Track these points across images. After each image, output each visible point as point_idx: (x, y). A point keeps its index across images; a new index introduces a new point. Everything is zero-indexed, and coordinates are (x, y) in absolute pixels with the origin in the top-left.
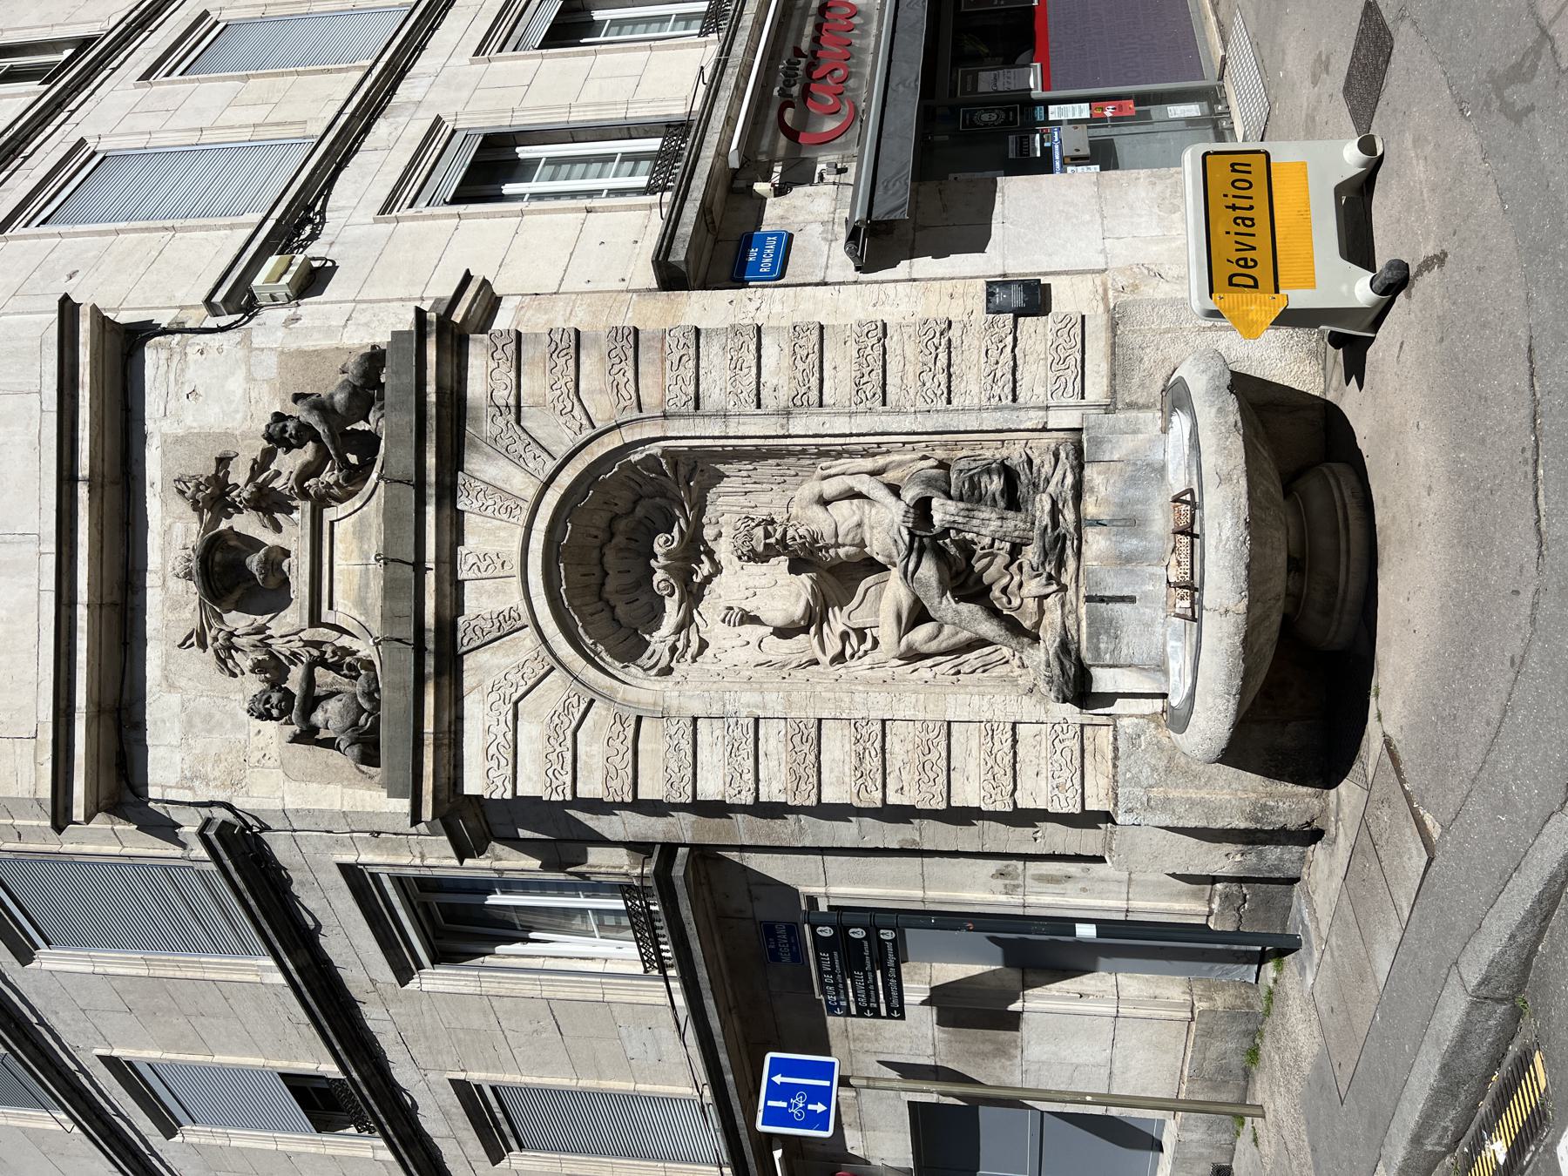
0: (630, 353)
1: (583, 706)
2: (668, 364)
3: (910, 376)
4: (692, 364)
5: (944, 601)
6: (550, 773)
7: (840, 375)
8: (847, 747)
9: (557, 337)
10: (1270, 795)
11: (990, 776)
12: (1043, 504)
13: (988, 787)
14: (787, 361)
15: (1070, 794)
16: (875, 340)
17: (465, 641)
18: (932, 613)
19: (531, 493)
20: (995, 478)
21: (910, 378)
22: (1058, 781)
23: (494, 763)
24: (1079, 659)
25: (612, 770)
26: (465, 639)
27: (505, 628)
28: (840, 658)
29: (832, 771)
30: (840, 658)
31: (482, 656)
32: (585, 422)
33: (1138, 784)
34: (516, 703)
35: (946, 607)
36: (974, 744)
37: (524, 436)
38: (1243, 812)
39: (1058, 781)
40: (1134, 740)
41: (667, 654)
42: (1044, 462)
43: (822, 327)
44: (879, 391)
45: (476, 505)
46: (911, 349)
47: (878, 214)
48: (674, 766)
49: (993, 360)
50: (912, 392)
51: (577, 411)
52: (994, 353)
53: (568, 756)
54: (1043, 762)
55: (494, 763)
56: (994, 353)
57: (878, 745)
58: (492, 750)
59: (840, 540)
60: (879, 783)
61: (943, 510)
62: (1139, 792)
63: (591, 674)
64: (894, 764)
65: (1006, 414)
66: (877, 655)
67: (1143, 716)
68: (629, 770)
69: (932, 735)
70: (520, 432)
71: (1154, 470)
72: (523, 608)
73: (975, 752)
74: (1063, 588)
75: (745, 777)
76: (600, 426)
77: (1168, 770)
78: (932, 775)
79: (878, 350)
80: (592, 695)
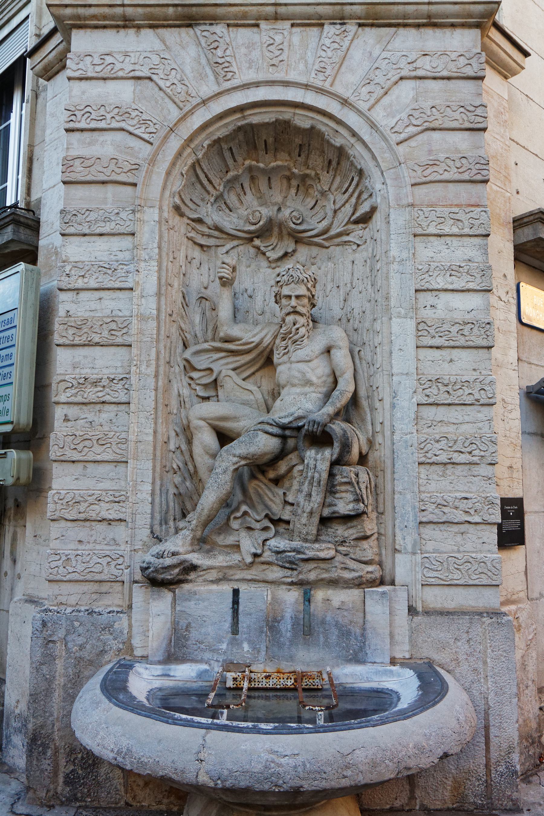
0: (466, 176)
1: (146, 136)
2: (456, 210)
3: (445, 429)
5: (235, 459)
6: (88, 109)
7: (446, 365)
8: (106, 371)
9: (479, 111)
10: (56, 751)
12: (325, 550)
13: (69, 498)
14: (458, 316)
16: (477, 396)
17: (205, 34)
18: (225, 448)
19: (339, 89)
23: (97, 61)
24: (180, 582)
25: (88, 163)
27: (220, 68)
28: (189, 367)
29: (85, 357)
30: (189, 367)
32: (403, 136)
33: (68, 633)
34: (150, 79)
35: (230, 458)
38: (42, 727)
41: (195, 216)
44: (431, 400)
45: (327, 42)
46: (466, 428)
48: (93, 216)
50: (430, 430)
51: (412, 130)
53: (102, 125)
54: (90, 546)
55: (97, 61)
56: (463, 505)
57: (107, 398)
58: (109, 59)
59: (294, 365)
60: (73, 399)
61: (318, 460)
63: (175, 144)
67: (130, 638)
68: (89, 178)
70: (394, 79)
71: (356, 654)
72: (236, 82)
73: (101, 486)
75: (80, 281)
77: (79, 659)
78: (80, 447)
79: (469, 400)
80: (156, 144)
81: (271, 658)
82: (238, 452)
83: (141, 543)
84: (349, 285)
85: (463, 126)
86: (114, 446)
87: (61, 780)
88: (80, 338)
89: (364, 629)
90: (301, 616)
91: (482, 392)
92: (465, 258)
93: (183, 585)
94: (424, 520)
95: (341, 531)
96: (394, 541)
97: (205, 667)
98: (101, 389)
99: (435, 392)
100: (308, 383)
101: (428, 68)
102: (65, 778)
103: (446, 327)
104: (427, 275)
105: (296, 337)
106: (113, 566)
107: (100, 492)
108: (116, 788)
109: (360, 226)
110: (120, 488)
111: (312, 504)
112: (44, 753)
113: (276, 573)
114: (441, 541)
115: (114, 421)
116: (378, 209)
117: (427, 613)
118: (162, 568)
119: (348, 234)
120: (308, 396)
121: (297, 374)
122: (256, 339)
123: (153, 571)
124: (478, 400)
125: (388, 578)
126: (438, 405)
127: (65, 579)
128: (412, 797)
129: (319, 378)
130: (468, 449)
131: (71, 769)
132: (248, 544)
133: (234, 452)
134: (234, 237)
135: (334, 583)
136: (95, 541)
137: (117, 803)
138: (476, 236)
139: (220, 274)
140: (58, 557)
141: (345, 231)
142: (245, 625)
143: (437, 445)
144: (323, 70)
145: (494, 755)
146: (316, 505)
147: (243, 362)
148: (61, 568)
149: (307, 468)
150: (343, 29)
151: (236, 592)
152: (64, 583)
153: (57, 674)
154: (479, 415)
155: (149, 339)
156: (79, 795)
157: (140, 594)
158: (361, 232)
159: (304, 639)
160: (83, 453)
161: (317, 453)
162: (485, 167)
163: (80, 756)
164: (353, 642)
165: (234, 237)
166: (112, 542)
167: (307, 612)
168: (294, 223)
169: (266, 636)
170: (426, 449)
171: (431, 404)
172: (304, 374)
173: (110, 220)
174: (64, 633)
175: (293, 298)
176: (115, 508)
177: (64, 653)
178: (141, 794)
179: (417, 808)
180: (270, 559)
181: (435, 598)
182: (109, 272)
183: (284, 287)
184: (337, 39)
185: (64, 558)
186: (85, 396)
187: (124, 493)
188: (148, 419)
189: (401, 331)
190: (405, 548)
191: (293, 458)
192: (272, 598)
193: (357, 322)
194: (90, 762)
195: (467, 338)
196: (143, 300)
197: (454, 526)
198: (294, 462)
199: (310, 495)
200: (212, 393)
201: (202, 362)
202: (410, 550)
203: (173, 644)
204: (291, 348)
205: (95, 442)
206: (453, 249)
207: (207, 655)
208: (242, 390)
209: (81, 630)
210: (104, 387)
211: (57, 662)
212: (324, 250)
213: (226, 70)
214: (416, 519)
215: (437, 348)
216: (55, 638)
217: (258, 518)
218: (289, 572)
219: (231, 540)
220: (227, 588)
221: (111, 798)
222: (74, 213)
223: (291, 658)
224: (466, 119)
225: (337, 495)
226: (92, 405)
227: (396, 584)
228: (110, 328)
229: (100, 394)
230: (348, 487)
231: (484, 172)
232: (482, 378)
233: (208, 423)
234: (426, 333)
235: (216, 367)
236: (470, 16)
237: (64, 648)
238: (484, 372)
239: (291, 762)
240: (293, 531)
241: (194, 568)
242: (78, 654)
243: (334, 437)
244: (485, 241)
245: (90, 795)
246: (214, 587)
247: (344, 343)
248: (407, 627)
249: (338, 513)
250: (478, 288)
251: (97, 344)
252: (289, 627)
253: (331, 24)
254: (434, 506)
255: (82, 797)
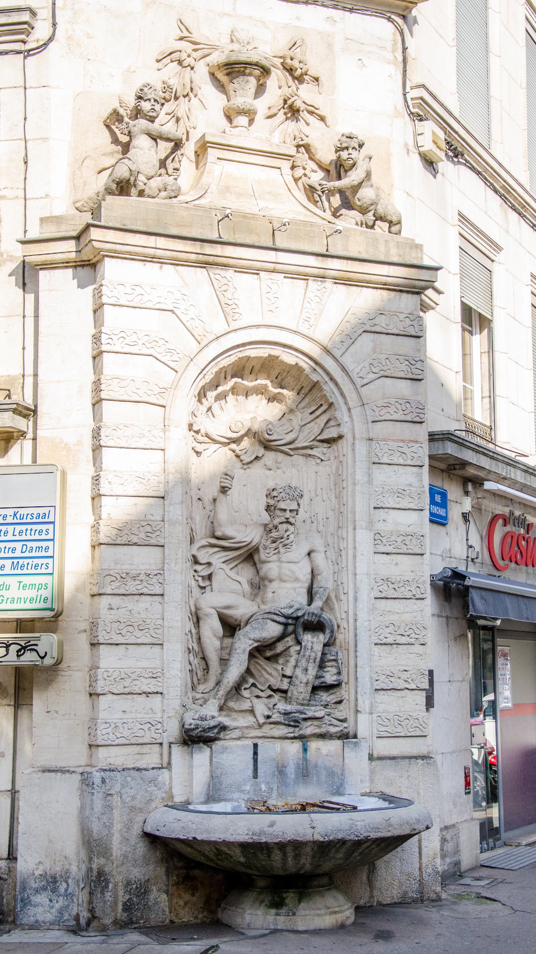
0: (409, 418)
1: (172, 364)
4: (401, 461)
8: (142, 567)
9: (419, 365)
10: (116, 885)
11: (123, 676)
13: (116, 675)
15: (111, 736)
16: (414, 593)
17: (217, 277)
20: (335, 678)
21: (394, 618)
22: (121, 726)
26: (217, 273)
27: (227, 309)
30: (196, 561)
31: (207, 289)
32: (366, 381)
33: (123, 786)
36: (145, 664)
37: (356, 335)
39: (121, 726)
40: (153, 781)
42: (340, 712)
43: (422, 555)
44: (383, 595)
46: (407, 617)
47: (474, 595)
49: (400, 675)
50: (381, 618)
51: (372, 376)
52: (405, 676)
54: (133, 715)
56: (405, 676)
57: (145, 591)
58: (139, 290)
59: (284, 565)
62: (117, 787)
64: (128, 603)
65: (368, 685)
66: (196, 591)
67: (171, 788)
69: (152, 632)
70: (359, 332)
71: (338, 788)
74: (260, 726)
76: (363, 391)
77: (132, 809)
78: (124, 632)
81: (280, 795)
82: (252, 636)
83: (174, 711)
84: (313, 493)
85: (407, 377)
86: (152, 632)
87: (120, 907)
88: (121, 539)
89: (343, 770)
90: (301, 762)
91: (418, 589)
92: (407, 483)
93: (217, 742)
94: (378, 687)
95: (324, 696)
96: (356, 705)
97: (236, 804)
98: (140, 583)
99: (386, 588)
100: (297, 580)
101: (384, 325)
102: (123, 906)
103: (394, 538)
104: (381, 496)
105: (287, 542)
106: (153, 731)
107: (140, 670)
108: (163, 909)
109: (325, 445)
110: (155, 666)
111: (308, 677)
112: (107, 887)
113: (282, 731)
114: (388, 703)
115: (149, 609)
116: (345, 438)
117: (380, 758)
118: (209, 728)
119: (312, 449)
120: (297, 591)
121: (288, 573)
122: (248, 539)
123: (201, 731)
124: (414, 596)
125: (351, 733)
126: (387, 598)
127: (114, 744)
128: (372, 897)
129: (305, 576)
130: (408, 633)
131: (128, 898)
132: (261, 708)
133: (250, 636)
134: (215, 441)
135: (322, 736)
136: (136, 712)
137: (163, 922)
138: (415, 466)
139: (223, 484)
140: (108, 725)
141: (311, 446)
142: (262, 771)
143: (387, 630)
144: (308, 319)
145: (424, 861)
146: (311, 677)
147: (231, 556)
148: (111, 734)
149: (305, 649)
150: (323, 286)
151: (256, 746)
152: (114, 747)
153: (115, 822)
154: (415, 606)
155: (176, 541)
156: (134, 919)
157: (178, 754)
158: (325, 449)
159: (303, 779)
160: (127, 637)
161: (313, 638)
162: (422, 411)
163: (134, 886)
164: (336, 779)
165: (215, 441)
166: (150, 711)
167: (305, 759)
168: (268, 434)
169: (277, 778)
170: (379, 633)
171: (382, 598)
172: (294, 572)
173: (144, 436)
174: (120, 788)
175: (288, 511)
176: (153, 683)
177: (119, 804)
178: (182, 913)
179: (375, 904)
180: (279, 720)
181: (385, 747)
182: (143, 481)
183: (280, 502)
184: (319, 294)
185: (113, 726)
186: (127, 589)
187: (160, 670)
188: (177, 608)
189: (364, 539)
190: (364, 710)
191: (290, 640)
192: (281, 749)
193: (321, 525)
194: (143, 891)
195: (408, 547)
196: (171, 507)
197: (398, 692)
198: (290, 643)
199: (306, 670)
200: (207, 583)
201: (203, 557)
202: (368, 711)
203: (211, 788)
204: (282, 550)
205: (136, 628)
206: (399, 475)
207: (236, 795)
208: (231, 581)
209: (132, 784)
210: (142, 581)
211: (114, 811)
212: (289, 457)
213: (234, 311)
214: (372, 687)
215: (387, 554)
216: (112, 792)
217: (263, 688)
218: (291, 729)
219: (246, 705)
220: (249, 743)
221: (159, 918)
222: (114, 427)
223: (294, 795)
224: (409, 370)
225: (326, 670)
226: (131, 596)
227: (358, 737)
228: (146, 531)
229: (139, 587)
230: (334, 663)
231: (422, 416)
232: (417, 578)
233: (217, 611)
234: (380, 542)
235: (213, 560)
236: (414, 287)
237: (119, 799)
238: (419, 574)
239: (363, 824)
240: (291, 698)
241: (224, 728)
242: (130, 804)
243: (326, 625)
244: (421, 471)
245: (143, 917)
246: (239, 742)
247: (322, 549)
248: (368, 769)
249: (325, 683)
250: (416, 508)
251: (135, 544)
252: (293, 770)
253: (314, 280)
254: (384, 677)
255: (137, 920)
